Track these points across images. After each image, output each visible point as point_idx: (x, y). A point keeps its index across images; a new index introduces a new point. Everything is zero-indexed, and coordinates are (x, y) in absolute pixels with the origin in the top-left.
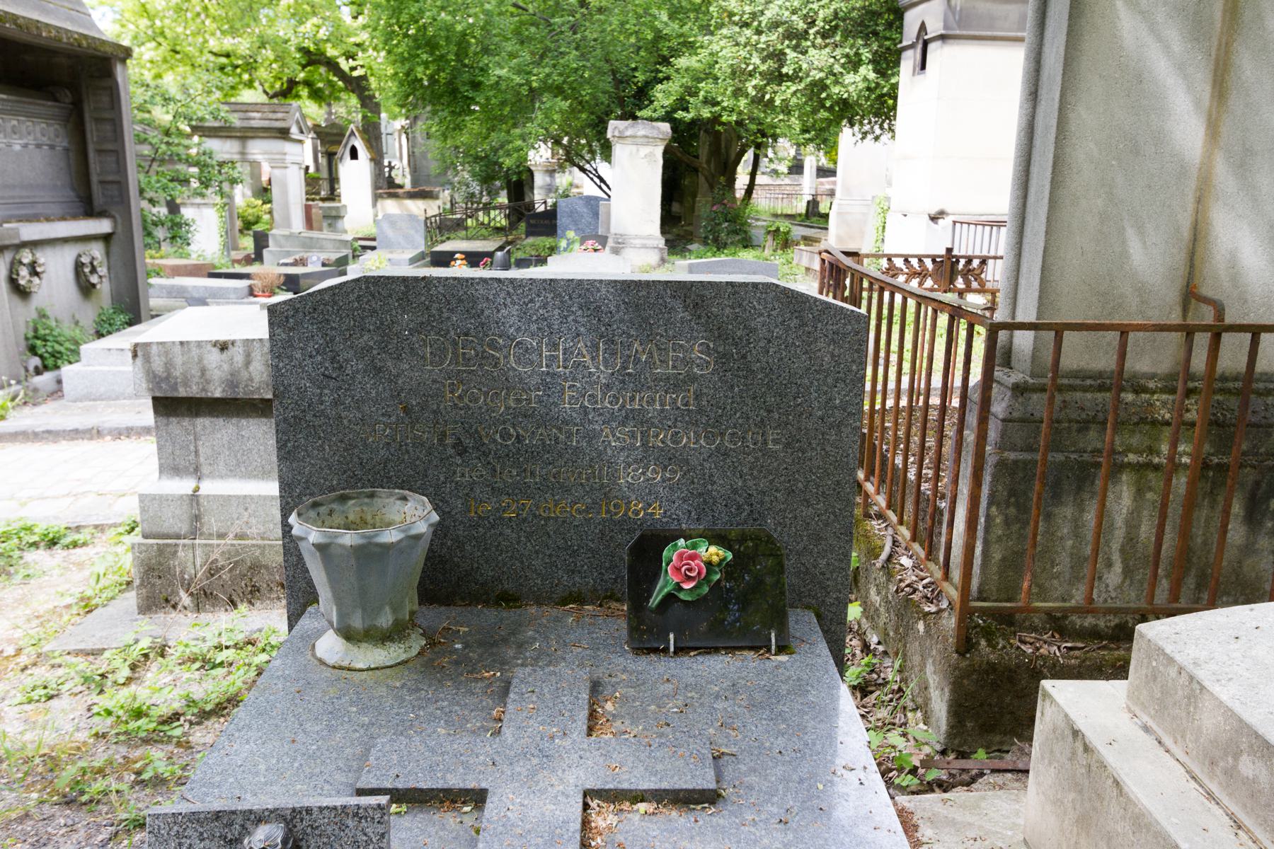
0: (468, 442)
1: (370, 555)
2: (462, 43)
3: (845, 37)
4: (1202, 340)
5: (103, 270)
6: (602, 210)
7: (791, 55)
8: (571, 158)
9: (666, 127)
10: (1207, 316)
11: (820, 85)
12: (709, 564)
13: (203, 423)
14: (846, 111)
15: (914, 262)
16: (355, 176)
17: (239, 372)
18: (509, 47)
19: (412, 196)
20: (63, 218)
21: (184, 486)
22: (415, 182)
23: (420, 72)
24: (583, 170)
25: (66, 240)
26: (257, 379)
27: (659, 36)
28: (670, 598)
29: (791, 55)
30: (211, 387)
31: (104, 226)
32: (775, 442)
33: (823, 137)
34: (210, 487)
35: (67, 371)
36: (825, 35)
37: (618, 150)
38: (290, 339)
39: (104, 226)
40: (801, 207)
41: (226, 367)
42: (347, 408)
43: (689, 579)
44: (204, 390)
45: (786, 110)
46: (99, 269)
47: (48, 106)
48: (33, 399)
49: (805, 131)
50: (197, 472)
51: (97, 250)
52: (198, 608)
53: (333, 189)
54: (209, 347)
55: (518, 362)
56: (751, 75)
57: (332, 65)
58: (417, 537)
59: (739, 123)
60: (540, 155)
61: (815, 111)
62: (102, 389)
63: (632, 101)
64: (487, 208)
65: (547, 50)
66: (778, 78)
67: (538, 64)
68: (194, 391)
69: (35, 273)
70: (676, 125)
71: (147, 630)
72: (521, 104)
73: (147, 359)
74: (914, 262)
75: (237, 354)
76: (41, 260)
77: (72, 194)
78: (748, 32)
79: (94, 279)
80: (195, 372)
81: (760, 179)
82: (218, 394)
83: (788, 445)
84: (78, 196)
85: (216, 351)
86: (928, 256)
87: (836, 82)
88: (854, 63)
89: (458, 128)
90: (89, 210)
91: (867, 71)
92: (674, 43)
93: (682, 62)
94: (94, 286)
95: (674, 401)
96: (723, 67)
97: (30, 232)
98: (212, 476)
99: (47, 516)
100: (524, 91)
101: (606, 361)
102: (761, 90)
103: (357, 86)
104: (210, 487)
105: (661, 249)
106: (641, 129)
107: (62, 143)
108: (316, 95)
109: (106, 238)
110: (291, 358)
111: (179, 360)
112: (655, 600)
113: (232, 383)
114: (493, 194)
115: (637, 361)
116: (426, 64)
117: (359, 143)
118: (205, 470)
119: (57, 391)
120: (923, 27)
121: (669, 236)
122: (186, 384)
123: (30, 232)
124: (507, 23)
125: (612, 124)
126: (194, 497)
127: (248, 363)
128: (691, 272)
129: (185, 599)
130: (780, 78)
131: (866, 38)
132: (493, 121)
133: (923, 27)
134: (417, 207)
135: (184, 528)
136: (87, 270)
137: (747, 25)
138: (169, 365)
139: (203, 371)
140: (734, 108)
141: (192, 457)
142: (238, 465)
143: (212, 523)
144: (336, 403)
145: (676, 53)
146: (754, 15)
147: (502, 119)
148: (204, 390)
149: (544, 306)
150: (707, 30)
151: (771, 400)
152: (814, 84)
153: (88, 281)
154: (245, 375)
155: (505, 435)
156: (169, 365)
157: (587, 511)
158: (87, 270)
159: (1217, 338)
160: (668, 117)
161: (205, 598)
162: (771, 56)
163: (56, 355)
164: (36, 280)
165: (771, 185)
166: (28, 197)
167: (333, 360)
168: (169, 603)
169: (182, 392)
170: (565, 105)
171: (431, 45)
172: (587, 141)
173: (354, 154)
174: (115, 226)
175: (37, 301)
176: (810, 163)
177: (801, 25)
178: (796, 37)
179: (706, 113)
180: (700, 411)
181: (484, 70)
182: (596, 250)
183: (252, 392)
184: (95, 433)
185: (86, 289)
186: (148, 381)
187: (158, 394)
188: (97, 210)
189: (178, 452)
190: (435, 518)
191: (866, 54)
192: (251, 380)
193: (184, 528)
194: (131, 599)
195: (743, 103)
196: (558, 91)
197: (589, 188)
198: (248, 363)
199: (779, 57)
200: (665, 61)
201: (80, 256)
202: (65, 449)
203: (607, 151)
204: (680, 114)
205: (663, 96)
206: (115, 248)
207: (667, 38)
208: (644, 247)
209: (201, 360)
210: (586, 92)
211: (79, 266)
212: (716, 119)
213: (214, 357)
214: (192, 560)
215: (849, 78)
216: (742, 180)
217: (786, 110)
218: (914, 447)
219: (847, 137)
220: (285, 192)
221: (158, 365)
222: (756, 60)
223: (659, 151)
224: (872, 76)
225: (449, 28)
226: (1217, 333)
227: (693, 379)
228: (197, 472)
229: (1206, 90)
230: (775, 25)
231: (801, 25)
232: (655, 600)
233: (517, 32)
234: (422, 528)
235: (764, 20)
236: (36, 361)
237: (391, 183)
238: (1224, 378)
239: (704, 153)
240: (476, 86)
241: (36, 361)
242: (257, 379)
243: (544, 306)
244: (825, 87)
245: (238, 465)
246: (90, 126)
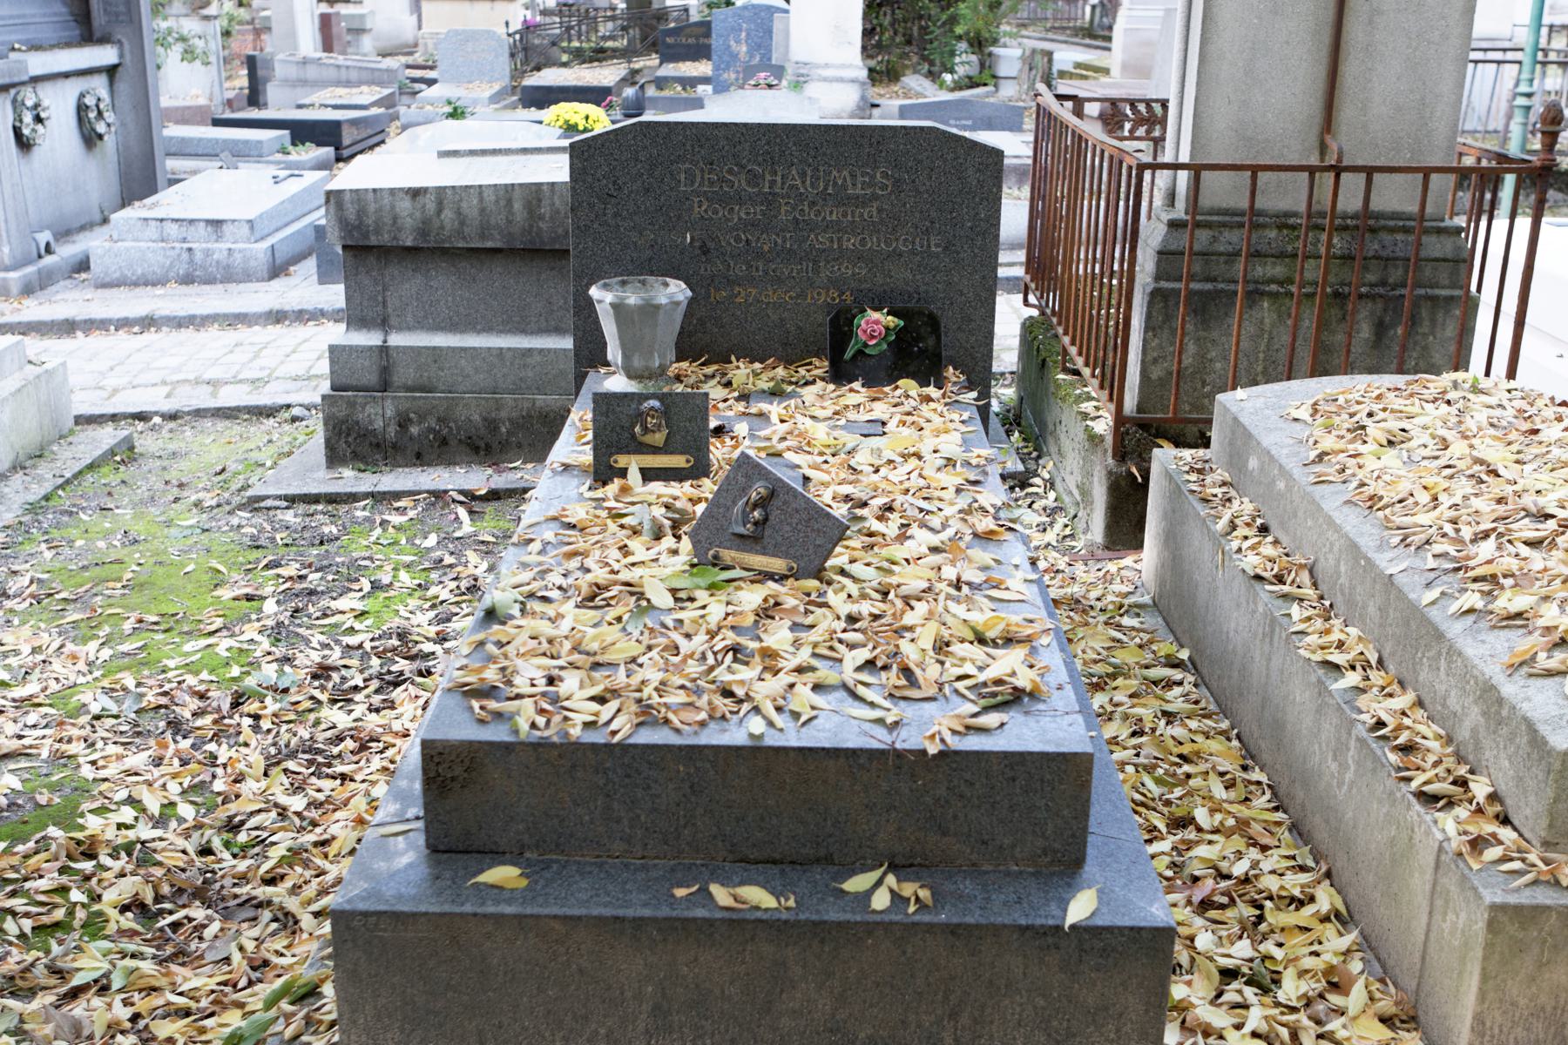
0: (711, 245)
5: (109, 116)
6: (777, 25)
12: (887, 328)
13: (393, 270)
15: (1142, 107)
17: (430, 220)
20: (68, 44)
21: (372, 339)
26: (448, 227)
28: (860, 353)
30: (403, 236)
31: (105, 55)
32: (937, 246)
34: (397, 340)
38: (584, 168)
39: (105, 55)
41: (418, 214)
42: (624, 219)
43: (873, 337)
44: (395, 238)
46: (106, 115)
51: (99, 85)
54: (401, 195)
55: (749, 183)
58: (678, 304)
62: (117, 275)
68: (385, 239)
69: (38, 120)
73: (340, 206)
74: (1142, 107)
75: (430, 203)
76: (45, 103)
77: (64, 10)
79: (101, 128)
80: (388, 220)
82: (409, 243)
83: (946, 248)
84: (72, 14)
85: (408, 198)
86: (1157, 101)
90: (88, 35)
94: (100, 137)
95: (862, 215)
97: (39, 63)
98: (400, 329)
101: (812, 184)
104: (397, 340)
105: (863, 84)
109: (111, 71)
110: (584, 181)
111: (372, 208)
112: (848, 355)
113: (423, 230)
115: (835, 183)
118: (393, 321)
121: (872, 63)
122: (377, 232)
123: (39, 63)
127: (439, 211)
128: (902, 117)
135: (372, 378)
136: (92, 115)
138: (362, 212)
139: (395, 219)
141: (380, 308)
142: (426, 317)
143: (398, 378)
144: (616, 215)
148: (395, 238)
149: (768, 143)
151: (933, 214)
153: (94, 130)
154: (436, 223)
155: (737, 239)
156: (362, 212)
157: (798, 296)
158: (92, 115)
159: (1337, 177)
164: (39, 127)
166: (19, 17)
167: (614, 183)
174: (121, 56)
180: (882, 220)
182: (770, 86)
183: (443, 241)
184: (149, 323)
185: (90, 139)
186: (341, 230)
187: (349, 243)
188: (97, 34)
189: (365, 303)
190: (689, 293)
192: (442, 227)
198: (439, 211)
201: (82, 96)
206: (122, 86)
208: (841, 80)
209: (393, 207)
211: (81, 109)
218: (1105, 291)
221: (351, 212)
227: (875, 197)
228: (384, 324)
232: (848, 355)
234: (681, 297)
238: (1345, 216)
242: (448, 227)
243: (768, 143)
245: (426, 317)
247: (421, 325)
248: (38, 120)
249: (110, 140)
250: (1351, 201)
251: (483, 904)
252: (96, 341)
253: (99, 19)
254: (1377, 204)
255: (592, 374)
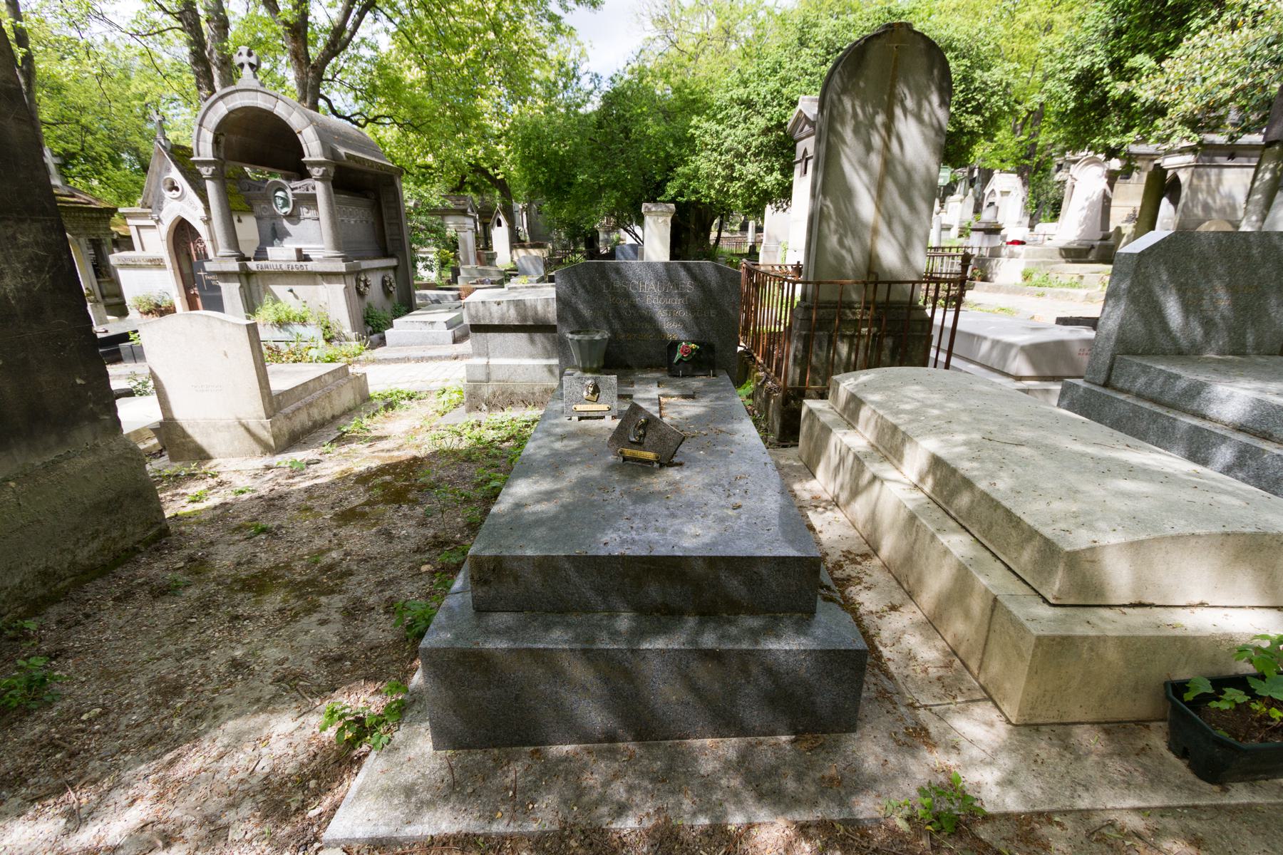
1: (592, 343)
2: (562, 161)
3: (766, 157)
4: (871, 287)
7: (738, 166)
8: (620, 224)
9: (672, 206)
10: (872, 279)
11: (753, 183)
14: (766, 197)
16: (500, 236)
18: (588, 162)
19: (533, 247)
20: (375, 258)
21: (483, 361)
22: (532, 239)
23: (541, 178)
24: (626, 230)
25: (377, 269)
27: (668, 155)
28: (680, 360)
29: (738, 166)
31: (393, 262)
33: (758, 211)
34: (493, 361)
35: (388, 333)
36: (755, 155)
37: (648, 219)
39: (393, 262)
40: (747, 250)
45: (735, 196)
47: (364, 201)
48: (373, 346)
49: (746, 207)
50: (487, 355)
52: (490, 410)
53: (487, 244)
56: (717, 177)
57: (484, 172)
59: (711, 203)
60: (601, 224)
61: (750, 196)
63: (654, 192)
64: (574, 252)
65: (608, 164)
66: (731, 179)
67: (602, 172)
68: (487, 322)
69: (366, 285)
70: (678, 205)
71: (473, 417)
72: (594, 194)
78: (715, 154)
81: (724, 234)
87: (762, 181)
88: (770, 170)
89: (561, 208)
90: (385, 254)
91: (777, 175)
92: (676, 160)
93: (680, 170)
96: (702, 172)
97: (365, 264)
99: (407, 388)
100: (596, 187)
102: (722, 186)
103: (502, 186)
104: (493, 361)
106: (662, 207)
107: (371, 220)
108: (476, 189)
109: (395, 268)
113: (502, 319)
114: (576, 244)
116: (543, 173)
117: (502, 217)
119: (382, 342)
120: (805, 151)
124: (586, 149)
125: (644, 205)
126: (488, 365)
129: (485, 407)
130: (732, 179)
131: (777, 156)
132: (579, 204)
133: (805, 151)
134: (535, 252)
135: (483, 378)
137: (715, 150)
140: (709, 194)
143: (493, 377)
145: (677, 165)
146: (719, 146)
147: (585, 203)
150: (693, 152)
152: (749, 182)
156: (477, 311)
160: (673, 200)
161: (492, 406)
162: (727, 167)
163: (378, 326)
165: (728, 239)
168: (478, 408)
169: (482, 322)
170: (618, 194)
171: (546, 163)
172: (631, 214)
173: (499, 224)
175: (368, 298)
176: (752, 224)
177: (743, 150)
178: (740, 157)
179: (693, 198)
181: (575, 176)
191: (777, 166)
193: (483, 378)
194: (463, 408)
195: (713, 192)
196: (614, 187)
197: (629, 240)
199: (731, 167)
200: (671, 169)
202: (393, 367)
203: (640, 220)
204: (680, 199)
205: (671, 190)
206: (399, 273)
207: (673, 156)
210: (629, 187)
211: (384, 282)
212: (699, 201)
213: (494, 308)
214: (486, 391)
215: (768, 178)
216: (714, 235)
217: (735, 196)
219: (769, 209)
220: (466, 245)
222: (719, 169)
223: (669, 219)
224: (779, 177)
225: (556, 153)
226: (876, 283)
228: (587, 332)
229: (874, 193)
230: (728, 151)
231: (743, 150)
233: (591, 154)
235: (724, 148)
236: (370, 329)
237: (519, 240)
239: (693, 219)
240: (570, 185)
241: (370, 329)
244: (756, 184)
246: (384, 210)
247: (502, 355)
248: (366, 285)
249: (395, 293)
250: (881, 297)
251: (492, 820)
252: (382, 367)
253: (390, 249)
254: (892, 298)
255: (989, 809)
